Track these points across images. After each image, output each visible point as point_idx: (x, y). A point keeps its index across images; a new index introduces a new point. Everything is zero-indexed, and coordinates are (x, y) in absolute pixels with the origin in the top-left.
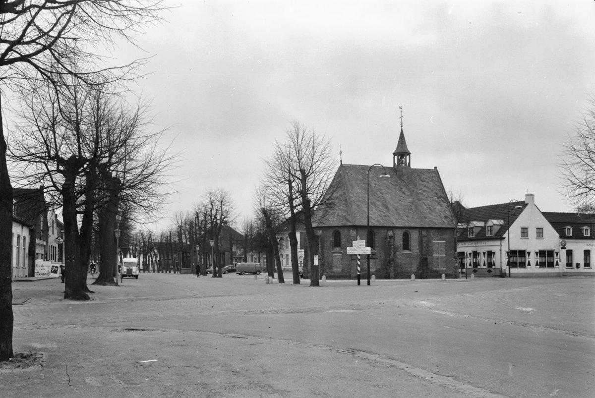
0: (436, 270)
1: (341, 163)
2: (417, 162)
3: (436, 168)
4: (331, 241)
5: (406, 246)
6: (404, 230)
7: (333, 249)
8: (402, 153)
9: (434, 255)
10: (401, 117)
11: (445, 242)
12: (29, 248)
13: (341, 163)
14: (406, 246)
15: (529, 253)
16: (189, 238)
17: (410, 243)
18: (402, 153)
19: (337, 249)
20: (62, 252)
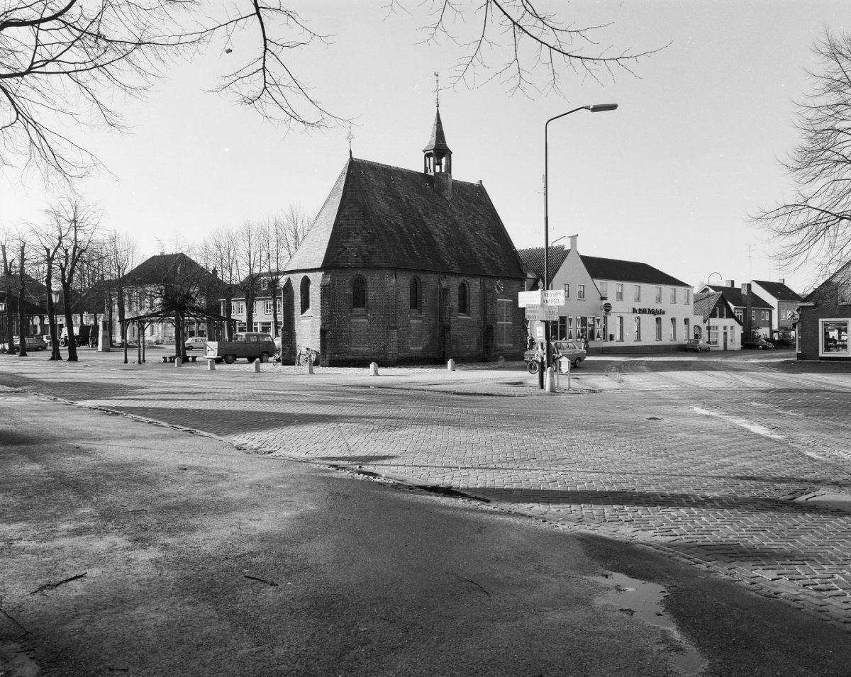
0: (501, 347)
1: (351, 156)
2: (463, 171)
3: (481, 181)
4: (346, 295)
5: (463, 308)
6: (303, 275)
7: (352, 311)
8: (440, 151)
9: (498, 322)
10: (437, 91)
11: (511, 300)
12: (842, 358)
13: (351, 156)
14: (463, 308)
15: (570, 320)
16: (264, 295)
17: (467, 303)
18: (440, 151)
19: (359, 310)
20: (720, 364)
